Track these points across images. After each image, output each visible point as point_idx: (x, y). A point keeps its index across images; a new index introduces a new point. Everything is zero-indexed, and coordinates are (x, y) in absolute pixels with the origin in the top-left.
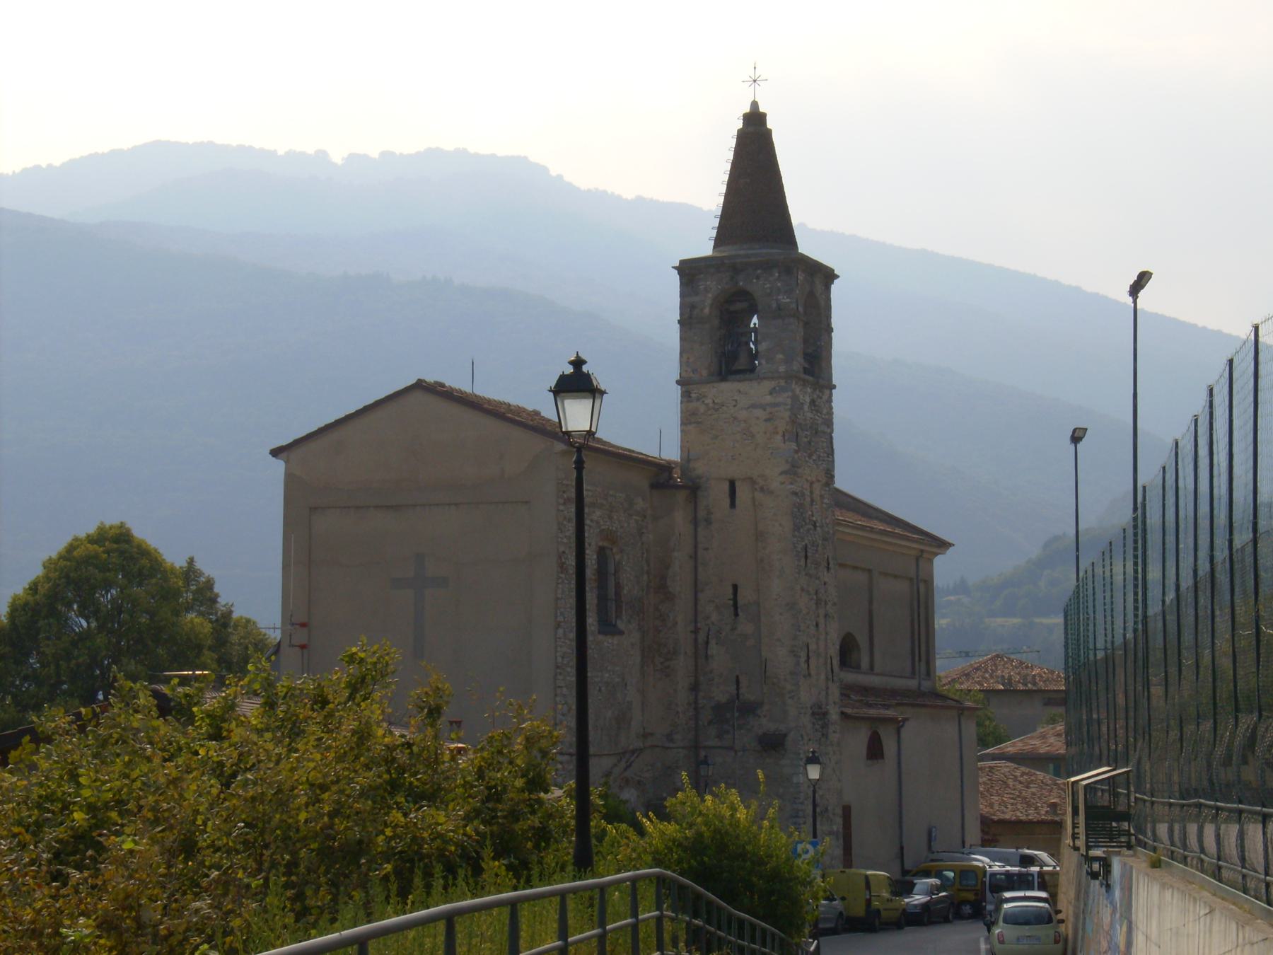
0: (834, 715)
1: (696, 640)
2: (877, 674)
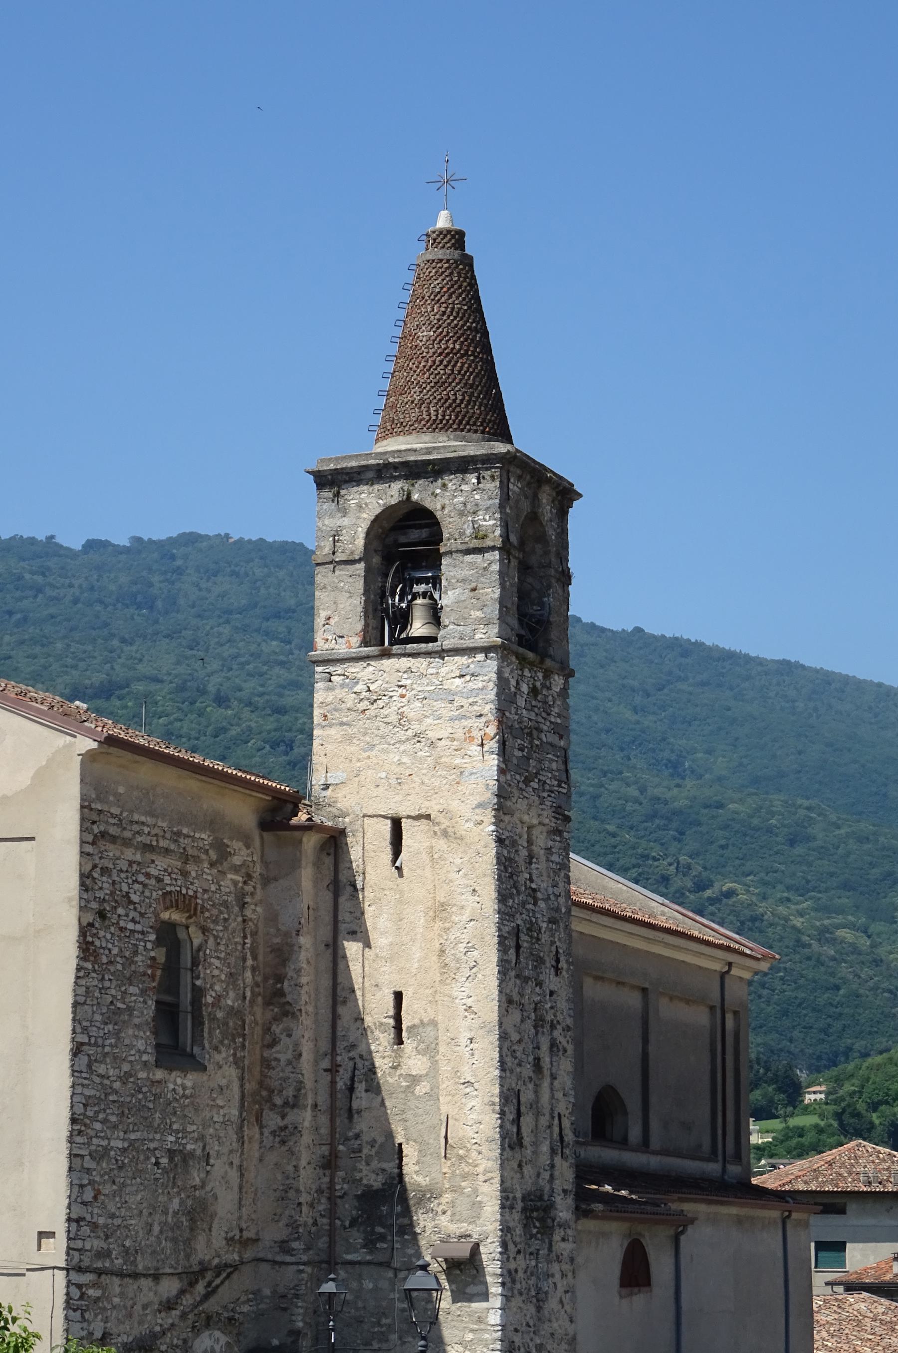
1: (333, 1083)
2: (655, 1153)
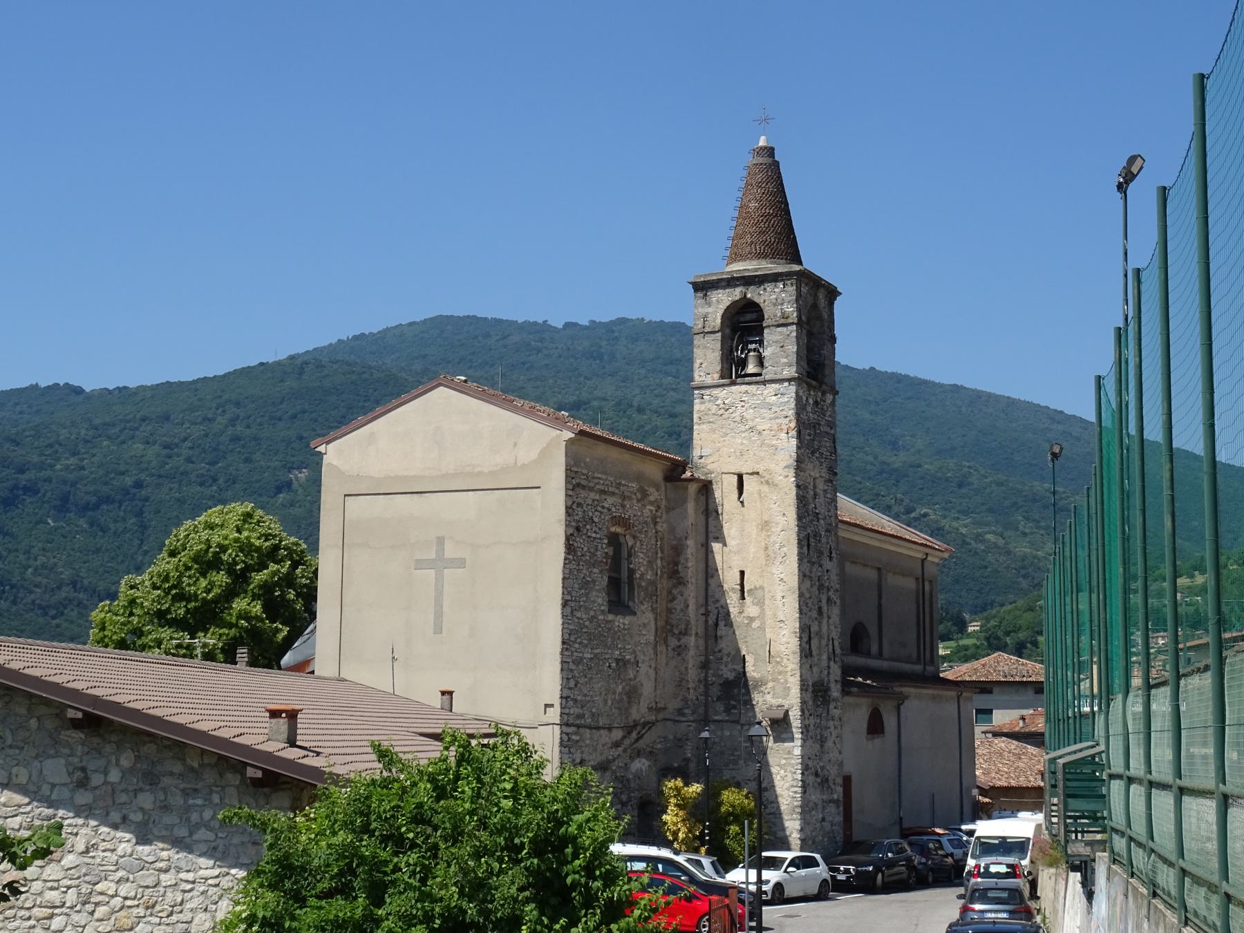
0: (835, 692)
1: (706, 621)
